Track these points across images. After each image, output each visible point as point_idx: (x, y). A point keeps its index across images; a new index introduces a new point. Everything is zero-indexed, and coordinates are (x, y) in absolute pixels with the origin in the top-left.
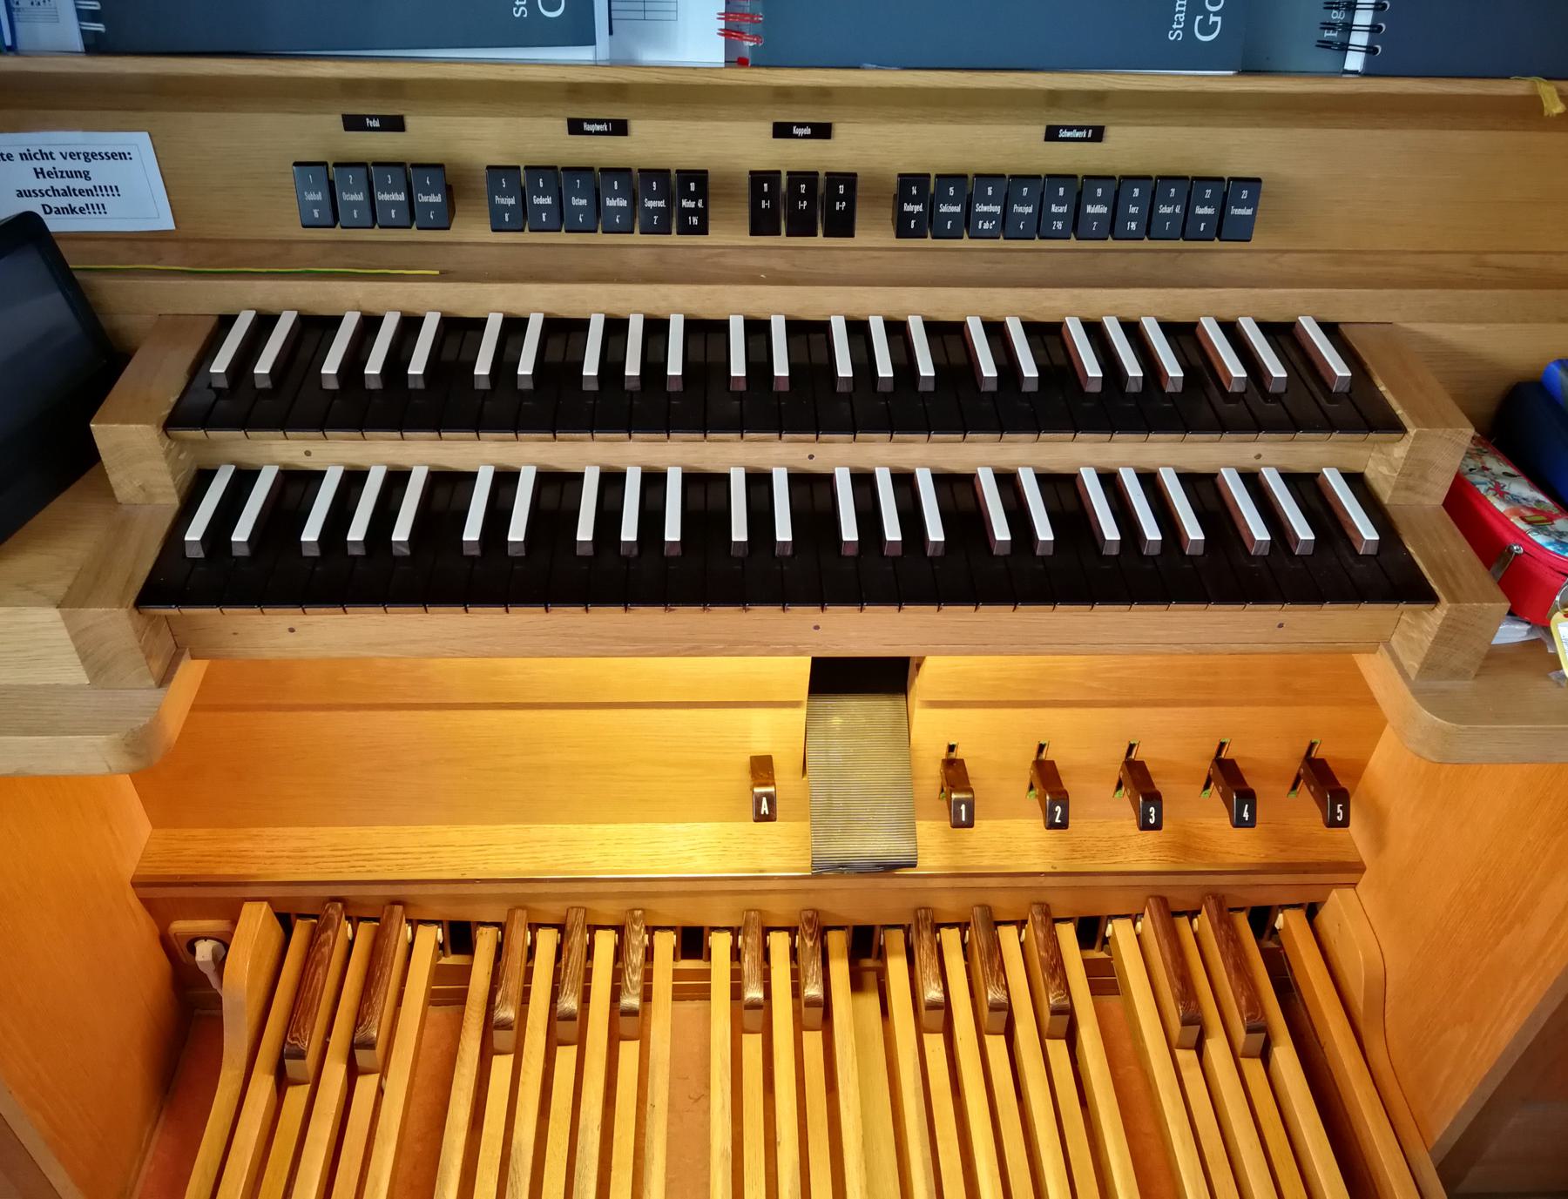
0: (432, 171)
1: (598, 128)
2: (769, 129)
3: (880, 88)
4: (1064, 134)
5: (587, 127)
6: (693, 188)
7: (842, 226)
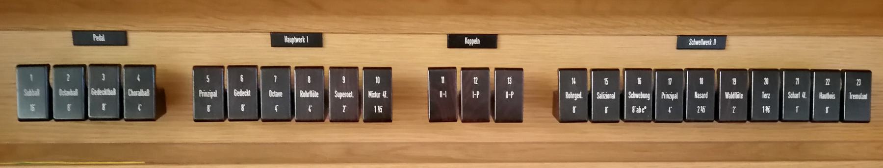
0: (72, 69)
1: (297, 40)
2: (444, 40)
3: (353, 13)
4: (693, 42)
5: (287, 40)
6: (242, 80)
7: (511, 115)
